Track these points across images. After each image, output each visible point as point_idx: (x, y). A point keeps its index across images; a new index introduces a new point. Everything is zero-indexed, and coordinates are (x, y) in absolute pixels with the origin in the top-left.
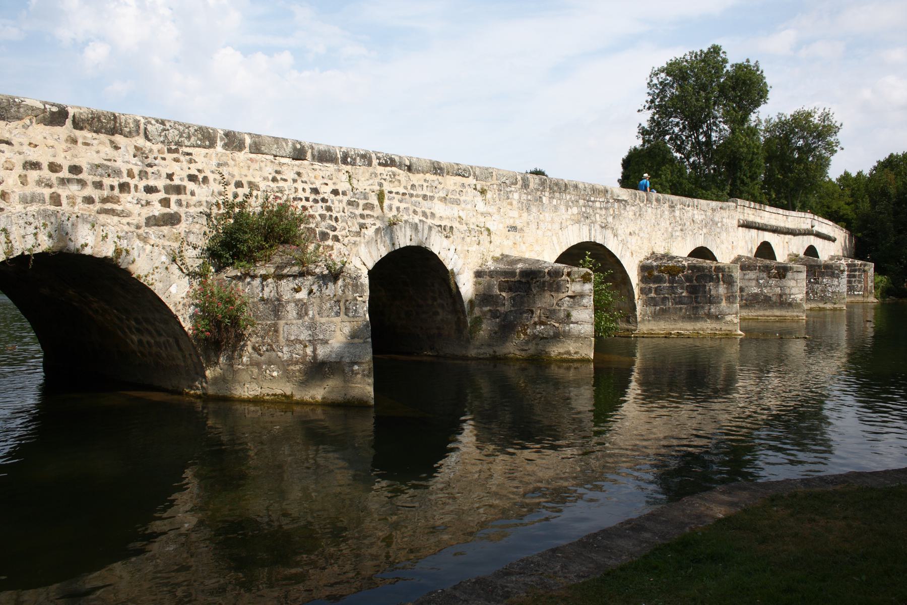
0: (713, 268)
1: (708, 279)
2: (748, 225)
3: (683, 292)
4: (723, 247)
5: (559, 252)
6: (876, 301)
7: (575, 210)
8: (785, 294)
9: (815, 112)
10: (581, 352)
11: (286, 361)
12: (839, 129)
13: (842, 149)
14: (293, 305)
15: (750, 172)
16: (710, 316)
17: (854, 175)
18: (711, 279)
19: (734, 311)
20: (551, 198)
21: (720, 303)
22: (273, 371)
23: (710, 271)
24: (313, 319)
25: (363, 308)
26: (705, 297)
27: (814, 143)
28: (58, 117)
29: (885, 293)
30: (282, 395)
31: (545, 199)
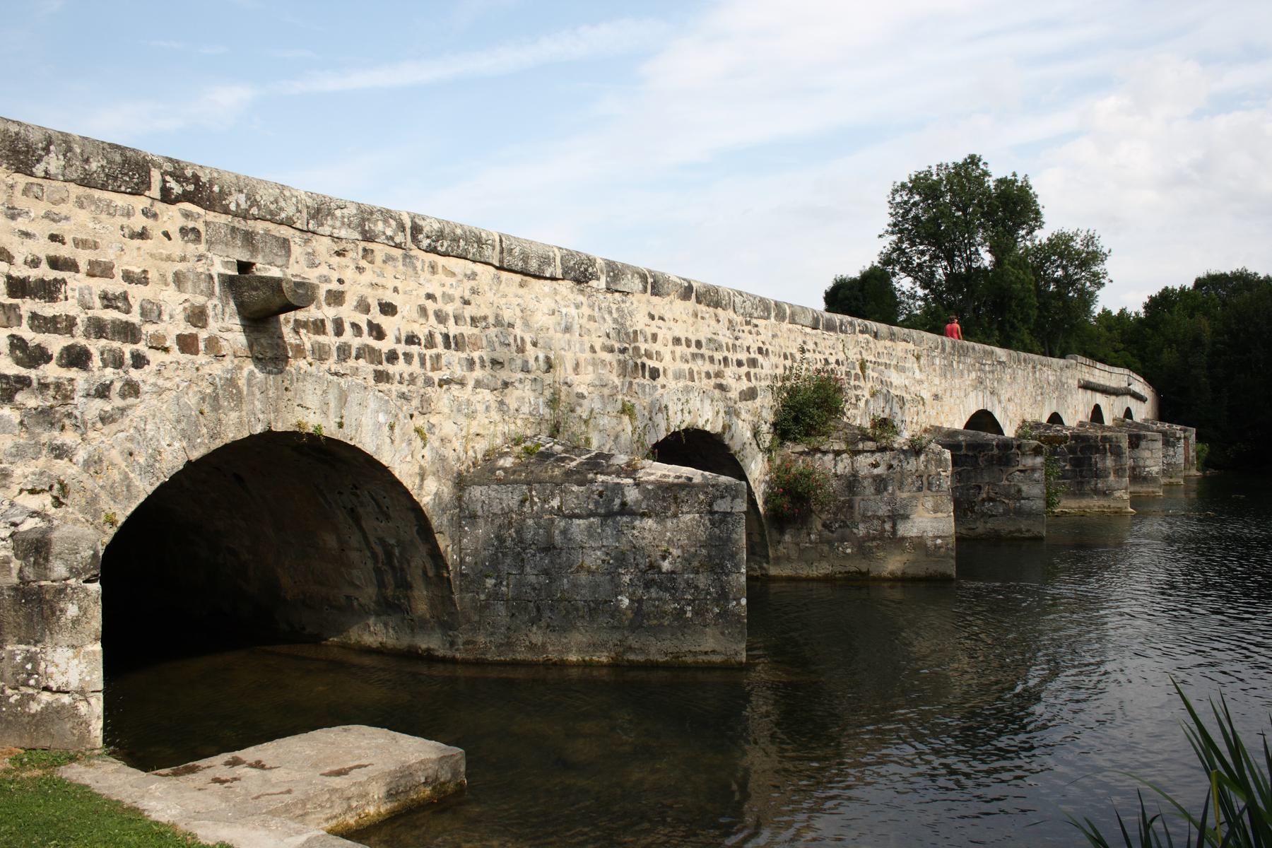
0: (1099, 438)
1: (1094, 450)
2: (1087, 386)
3: (1065, 466)
4: (1069, 411)
5: (965, 422)
6: (1198, 474)
7: (973, 375)
8: (1139, 467)
11: (862, 537)
12: (1106, 256)
13: (1111, 281)
14: (870, 480)
15: (1022, 313)
16: (1097, 492)
17: (1115, 312)
18: (1097, 450)
19: (1124, 485)
20: (959, 362)
21: (1107, 477)
22: (847, 548)
23: (1096, 441)
24: (893, 494)
25: (947, 482)
26: (1091, 470)
27: (1076, 274)
28: (687, 292)
29: (1205, 464)
30: (856, 572)
31: (955, 363)
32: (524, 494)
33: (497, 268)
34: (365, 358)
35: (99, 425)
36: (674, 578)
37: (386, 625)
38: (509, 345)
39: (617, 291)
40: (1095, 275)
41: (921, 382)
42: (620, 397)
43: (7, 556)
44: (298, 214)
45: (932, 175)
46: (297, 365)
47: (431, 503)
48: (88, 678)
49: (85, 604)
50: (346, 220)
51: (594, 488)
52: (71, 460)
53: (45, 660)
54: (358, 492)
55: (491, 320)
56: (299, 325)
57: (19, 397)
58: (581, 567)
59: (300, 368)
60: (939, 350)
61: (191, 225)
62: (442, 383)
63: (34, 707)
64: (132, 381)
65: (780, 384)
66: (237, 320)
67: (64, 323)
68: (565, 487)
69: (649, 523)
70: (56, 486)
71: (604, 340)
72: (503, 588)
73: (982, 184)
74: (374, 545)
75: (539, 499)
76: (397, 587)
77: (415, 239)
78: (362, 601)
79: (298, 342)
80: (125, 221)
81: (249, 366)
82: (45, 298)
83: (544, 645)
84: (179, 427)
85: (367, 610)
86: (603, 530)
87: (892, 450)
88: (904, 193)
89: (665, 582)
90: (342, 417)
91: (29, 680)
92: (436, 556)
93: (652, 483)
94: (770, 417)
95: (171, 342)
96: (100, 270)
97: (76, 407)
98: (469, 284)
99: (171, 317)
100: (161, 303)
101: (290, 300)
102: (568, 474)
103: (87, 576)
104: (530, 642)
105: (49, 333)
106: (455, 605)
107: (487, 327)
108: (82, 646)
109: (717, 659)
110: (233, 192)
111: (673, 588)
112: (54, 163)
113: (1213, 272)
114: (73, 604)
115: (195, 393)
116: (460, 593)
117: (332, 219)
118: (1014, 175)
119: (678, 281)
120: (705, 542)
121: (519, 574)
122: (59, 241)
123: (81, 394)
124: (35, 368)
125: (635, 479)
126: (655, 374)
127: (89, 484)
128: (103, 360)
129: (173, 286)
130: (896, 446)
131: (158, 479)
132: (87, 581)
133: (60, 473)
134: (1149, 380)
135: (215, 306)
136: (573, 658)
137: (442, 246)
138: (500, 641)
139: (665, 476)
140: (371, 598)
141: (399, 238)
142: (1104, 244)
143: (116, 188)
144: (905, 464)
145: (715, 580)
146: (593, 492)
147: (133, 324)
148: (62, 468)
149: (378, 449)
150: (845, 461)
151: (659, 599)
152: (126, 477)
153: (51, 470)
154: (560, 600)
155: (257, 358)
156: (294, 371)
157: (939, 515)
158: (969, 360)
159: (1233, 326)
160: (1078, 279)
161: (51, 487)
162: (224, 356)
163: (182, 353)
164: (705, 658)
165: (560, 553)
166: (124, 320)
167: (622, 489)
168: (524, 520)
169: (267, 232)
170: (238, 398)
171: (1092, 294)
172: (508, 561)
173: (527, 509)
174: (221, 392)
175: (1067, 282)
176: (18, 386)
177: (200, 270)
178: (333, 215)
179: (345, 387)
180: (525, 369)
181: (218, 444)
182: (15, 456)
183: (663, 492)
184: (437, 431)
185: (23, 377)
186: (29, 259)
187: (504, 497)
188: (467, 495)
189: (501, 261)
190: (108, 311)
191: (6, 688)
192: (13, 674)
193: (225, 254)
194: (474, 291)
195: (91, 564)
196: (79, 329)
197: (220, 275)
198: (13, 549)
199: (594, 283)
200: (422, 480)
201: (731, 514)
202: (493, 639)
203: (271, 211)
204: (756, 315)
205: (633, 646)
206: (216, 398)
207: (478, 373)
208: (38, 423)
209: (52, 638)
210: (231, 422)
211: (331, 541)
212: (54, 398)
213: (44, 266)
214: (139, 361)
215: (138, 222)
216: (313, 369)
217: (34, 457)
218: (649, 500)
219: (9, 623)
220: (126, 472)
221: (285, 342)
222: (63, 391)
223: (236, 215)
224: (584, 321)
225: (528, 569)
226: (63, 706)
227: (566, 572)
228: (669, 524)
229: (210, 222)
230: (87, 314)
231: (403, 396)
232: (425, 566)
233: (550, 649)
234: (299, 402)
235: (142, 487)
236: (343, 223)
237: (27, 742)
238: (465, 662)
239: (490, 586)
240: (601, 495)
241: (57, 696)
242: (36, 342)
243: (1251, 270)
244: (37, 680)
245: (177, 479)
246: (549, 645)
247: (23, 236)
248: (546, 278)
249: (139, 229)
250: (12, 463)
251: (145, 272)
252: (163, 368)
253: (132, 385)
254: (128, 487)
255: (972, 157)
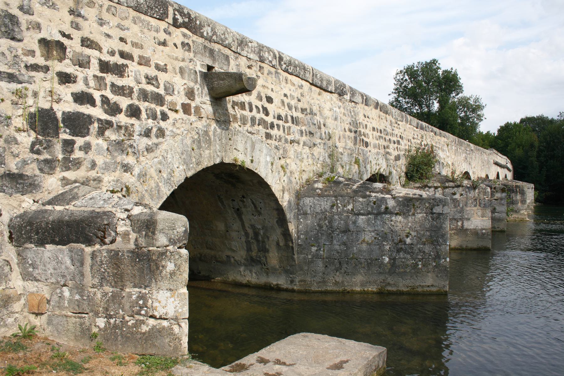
2: (496, 164)
7: (464, 155)
9: (471, 97)
10: (500, 227)
18: (513, 192)
19: (525, 208)
21: (517, 204)
32: (333, 202)
33: (311, 84)
34: (262, 125)
35: (145, 153)
36: (412, 247)
37: (251, 271)
38: (315, 124)
39: (353, 102)
40: (479, 115)
41: (448, 157)
42: (354, 155)
43: (127, 230)
44: (233, 43)
45: (414, 67)
46: (235, 126)
47: (287, 206)
48: (180, 310)
49: (179, 262)
50: (253, 49)
51: (371, 200)
52: (131, 174)
53: (152, 299)
54: (245, 200)
55: (308, 111)
56: (235, 104)
57: (107, 133)
58: (364, 241)
59: (236, 128)
60: (454, 143)
61: (186, 41)
62: (292, 142)
63: (144, 328)
64: (161, 128)
65: (407, 154)
66: (208, 98)
67: (128, 91)
68: (356, 199)
69: (400, 218)
70: (125, 189)
71: (348, 126)
72: (321, 252)
73: (437, 72)
74: (247, 229)
75: (341, 205)
76: (259, 251)
77: (280, 65)
78: (236, 258)
79: (234, 113)
80: (154, 34)
81: (214, 125)
82: (118, 75)
83: (343, 282)
84: (182, 157)
85: (239, 263)
86: (375, 222)
87: (463, 187)
88: (401, 75)
89: (408, 249)
90: (252, 157)
91: (141, 311)
92: (286, 234)
93: (401, 197)
94: (404, 169)
95: (179, 107)
96: (144, 62)
97: (135, 142)
98: (300, 91)
99: (179, 93)
100: (174, 84)
101: (246, 86)
102: (355, 192)
103: (181, 244)
104: (335, 281)
105: (121, 96)
106: (295, 261)
107: (306, 115)
108: (176, 290)
109: (434, 289)
110: (205, 25)
111: (412, 252)
112: (76, 13)
113: (528, 116)
114: (171, 262)
115: (190, 137)
116: (297, 255)
117: (247, 47)
118: (452, 69)
119: (374, 100)
120: (429, 228)
121: (330, 245)
122: (124, 42)
123: (137, 133)
124: (114, 116)
125: (392, 195)
126: (367, 145)
127: (140, 188)
128: (147, 114)
129: (179, 74)
130: (464, 185)
131: (172, 187)
132: (180, 248)
133: (126, 181)
134: (512, 163)
135: (198, 88)
136: (358, 289)
137: (290, 69)
138: (319, 280)
139: (408, 194)
140: (242, 257)
141: (274, 63)
142: (483, 102)
143: (152, 15)
144: (468, 194)
145: (433, 248)
146: (370, 202)
147: (161, 95)
148: (129, 179)
149: (266, 175)
150: (440, 191)
151: (404, 258)
152: (158, 186)
153: (122, 179)
154: (352, 258)
155: (217, 120)
156: (233, 130)
157: (484, 218)
158: (463, 148)
159: (548, 139)
160: (471, 117)
161: (122, 189)
162: (202, 118)
163: (184, 114)
164: (428, 289)
165: (352, 234)
166: (157, 92)
167: (386, 200)
168: (333, 216)
169: (220, 50)
170: (209, 142)
171: (477, 124)
172: (324, 238)
173: (334, 210)
174: (202, 138)
175: (466, 118)
176: (107, 126)
177: (191, 67)
178: (248, 45)
179: (254, 140)
180: (321, 138)
181: (200, 168)
182: (104, 169)
183: (407, 202)
184: (289, 167)
185: (109, 121)
186: (110, 51)
187: (322, 203)
188: (302, 202)
189: (313, 80)
190: (149, 85)
191: (126, 316)
192: (130, 307)
193: (201, 60)
194: (302, 95)
195: (183, 236)
196: (135, 95)
197: (200, 72)
198: (131, 226)
199: (345, 96)
200: (283, 193)
201: (442, 214)
202: (315, 279)
203: (222, 39)
204: (399, 120)
205: (390, 283)
206: (199, 142)
207: (304, 138)
208: (116, 150)
209: (156, 284)
210: (206, 156)
211: (221, 227)
212: (124, 135)
213: (117, 55)
214: (165, 117)
215: (162, 36)
216: (240, 129)
217: (114, 170)
218: (400, 206)
219: (128, 274)
220: (158, 182)
221: (229, 113)
222: (128, 131)
223: (206, 39)
224: (342, 115)
225: (335, 242)
226: (164, 328)
227: (355, 244)
228: (410, 219)
229: (195, 41)
230: (138, 86)
231: (277, 148)
232: (278, 240)
233: (346, 284)
234: (235, 147)
235: (165, 191)
236: (252, 50)
237: (140, 350)
238: (300, 292)
239: (314, 251)
240: (374, 203)
241: (159, 321)
242: (114, 100)
243: (545, 115)
244: (146, 311)
245: (181, 186)
246: (345, 282)
247: (106, 36)
248: (328, 92)
249: (162, 40)
250: (103, 174)
251: (166, 65)
252: (175, 122)
253: (161, 131)
254: (159, 191)
255: (434, 60)
